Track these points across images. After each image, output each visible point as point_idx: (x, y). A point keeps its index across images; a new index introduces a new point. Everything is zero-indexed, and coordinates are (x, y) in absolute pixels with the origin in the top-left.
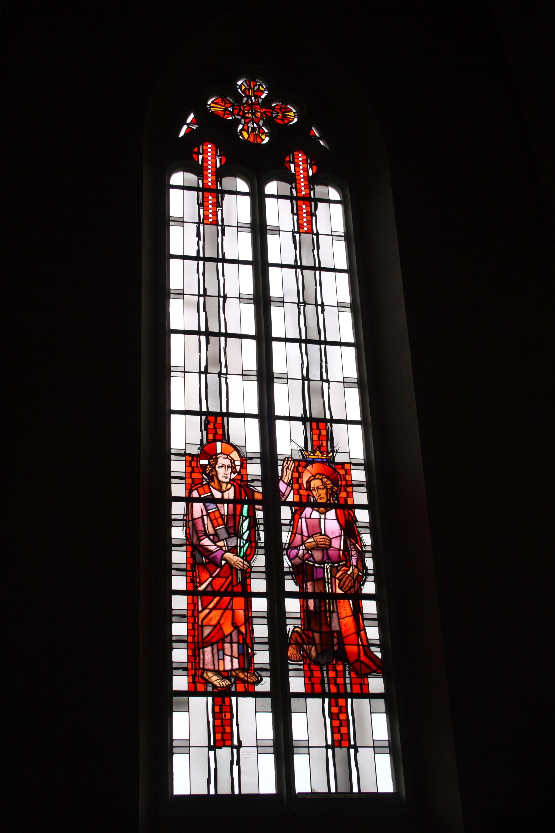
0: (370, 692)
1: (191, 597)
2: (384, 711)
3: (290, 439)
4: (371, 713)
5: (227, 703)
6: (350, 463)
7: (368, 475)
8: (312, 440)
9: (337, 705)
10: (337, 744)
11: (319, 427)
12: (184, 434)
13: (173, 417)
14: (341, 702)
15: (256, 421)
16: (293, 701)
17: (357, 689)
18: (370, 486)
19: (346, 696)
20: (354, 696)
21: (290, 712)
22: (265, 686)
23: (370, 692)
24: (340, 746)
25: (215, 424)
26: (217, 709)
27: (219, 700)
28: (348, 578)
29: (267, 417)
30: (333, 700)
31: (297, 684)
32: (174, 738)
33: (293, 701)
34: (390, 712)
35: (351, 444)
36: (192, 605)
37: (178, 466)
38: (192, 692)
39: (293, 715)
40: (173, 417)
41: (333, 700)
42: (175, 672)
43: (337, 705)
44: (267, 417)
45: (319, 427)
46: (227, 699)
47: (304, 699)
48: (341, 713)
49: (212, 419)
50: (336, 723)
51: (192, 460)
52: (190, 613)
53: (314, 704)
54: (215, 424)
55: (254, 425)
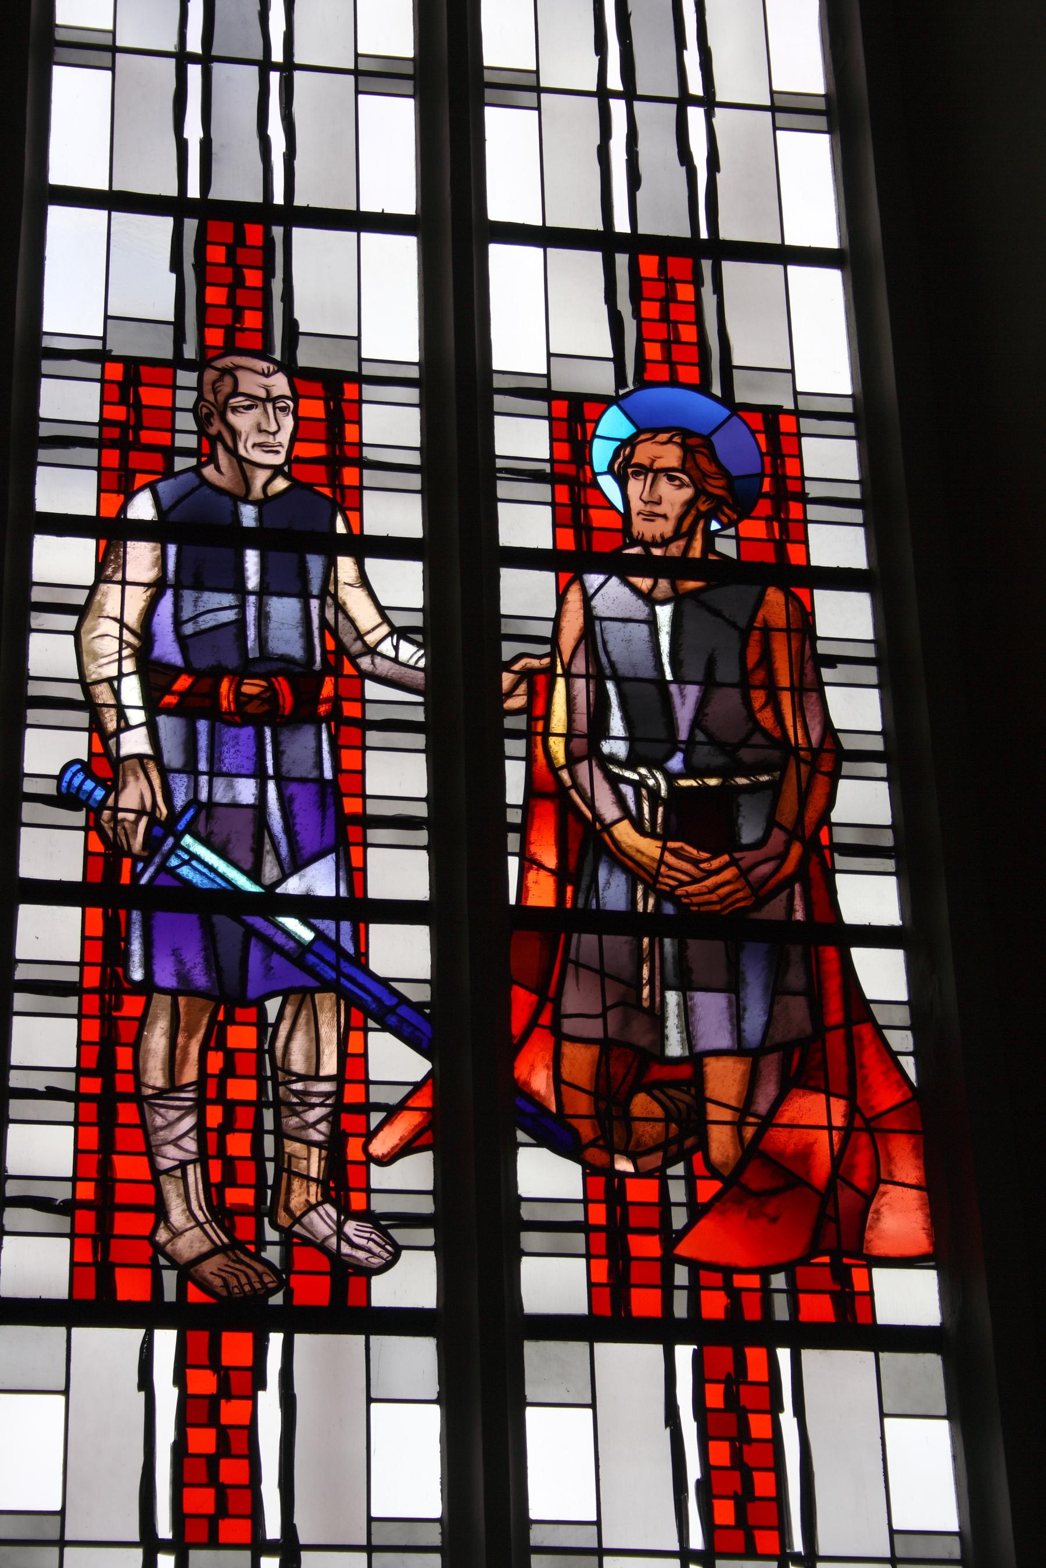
0: (375, 1303)
1: (96, 913)
2: (432, 1390)
3: (543, 317)
4: (370, 1400)
5: (757, 1372)
6: (798, 413)
7: (869, 459)
8: (202, 306)
9: (214, 1363)
10: (197, 1530)
11: (667, 279)
12: (100, 279)
13: (57, 216)
14: (235, 1348)
15: (405, 248)
16: (536, 1354)
17: (818, 1308)
18: (876, 502)
19: (772, 1335)
20: (805, 1336)
21: (521, 1403)
22: (411, 1281)
23: (375, 1303)
24: (213, 1542)
25: (232, 249)
26: (715, 1396)
27: (722, 1357)
28: (674, 852)
29: (453, 230)
30: (200, 1338)
31: (553, 1281)
32: (533, 1515)
33: (536, 1354)
34: (964, 1413)
35: (804, 337)
36: (105, 949)
37: (69, 400)
38: (607, 1320)
39: (532, 1415)
40: (57, 216)
41: (200, 1338)
42: (529, 1240)
43: (214, 1363)
44: (453, 230)
45: (667, 279)
46: (755, 1356)
47: (583, 1347)
48: (229, 1397)
49: (222, 230)
50: (204, 1441)
51: (127, 378)
52: (93, 977)
53: (631, 1368)
54: (232, 249)
55: (396, 260)
